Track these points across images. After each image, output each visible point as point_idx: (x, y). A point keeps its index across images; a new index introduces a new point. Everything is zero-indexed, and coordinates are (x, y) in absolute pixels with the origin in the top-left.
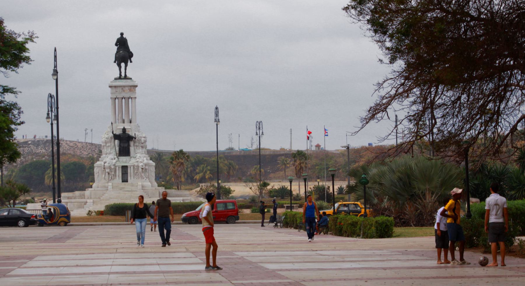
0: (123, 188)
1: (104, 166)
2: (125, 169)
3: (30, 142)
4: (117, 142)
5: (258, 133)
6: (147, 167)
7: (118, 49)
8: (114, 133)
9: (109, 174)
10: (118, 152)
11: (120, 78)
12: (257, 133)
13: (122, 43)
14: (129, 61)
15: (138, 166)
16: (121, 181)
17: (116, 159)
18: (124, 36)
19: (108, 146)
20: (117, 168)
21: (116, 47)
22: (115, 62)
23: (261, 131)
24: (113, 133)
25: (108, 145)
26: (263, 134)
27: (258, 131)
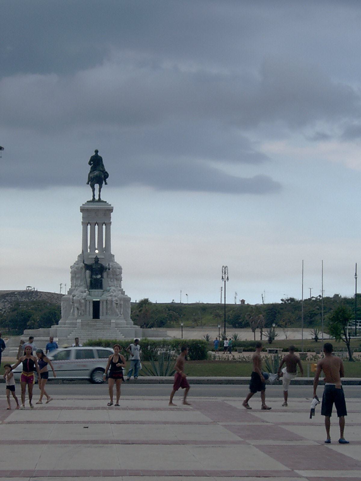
0: (95, 325)
1: (73, 300)
2: (96, 305)
3: (16, 293)
4: (88, 272)
5: (224, 277)
6: (122, 302)
7: (92, 168)
8: (86, 263)
9: (78, 309)
10: (89, 284)
11: (94, 200)
12: (222, 277)
13: (96, 162)
14: (104, 183)
15: (112, 301)
16: (92, 317)
17: (87, 292)
18: (99, 154)
19: (78, 278)
20: (88, 303)
21: (90, 166)
22: (88, 184)
23: (226, 276)
24: (83, 262)
25: (77, 276)
26: (228, 279)
27: (224, 276)
